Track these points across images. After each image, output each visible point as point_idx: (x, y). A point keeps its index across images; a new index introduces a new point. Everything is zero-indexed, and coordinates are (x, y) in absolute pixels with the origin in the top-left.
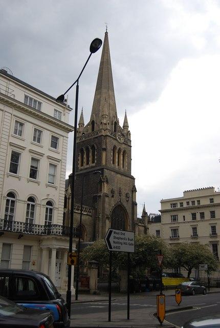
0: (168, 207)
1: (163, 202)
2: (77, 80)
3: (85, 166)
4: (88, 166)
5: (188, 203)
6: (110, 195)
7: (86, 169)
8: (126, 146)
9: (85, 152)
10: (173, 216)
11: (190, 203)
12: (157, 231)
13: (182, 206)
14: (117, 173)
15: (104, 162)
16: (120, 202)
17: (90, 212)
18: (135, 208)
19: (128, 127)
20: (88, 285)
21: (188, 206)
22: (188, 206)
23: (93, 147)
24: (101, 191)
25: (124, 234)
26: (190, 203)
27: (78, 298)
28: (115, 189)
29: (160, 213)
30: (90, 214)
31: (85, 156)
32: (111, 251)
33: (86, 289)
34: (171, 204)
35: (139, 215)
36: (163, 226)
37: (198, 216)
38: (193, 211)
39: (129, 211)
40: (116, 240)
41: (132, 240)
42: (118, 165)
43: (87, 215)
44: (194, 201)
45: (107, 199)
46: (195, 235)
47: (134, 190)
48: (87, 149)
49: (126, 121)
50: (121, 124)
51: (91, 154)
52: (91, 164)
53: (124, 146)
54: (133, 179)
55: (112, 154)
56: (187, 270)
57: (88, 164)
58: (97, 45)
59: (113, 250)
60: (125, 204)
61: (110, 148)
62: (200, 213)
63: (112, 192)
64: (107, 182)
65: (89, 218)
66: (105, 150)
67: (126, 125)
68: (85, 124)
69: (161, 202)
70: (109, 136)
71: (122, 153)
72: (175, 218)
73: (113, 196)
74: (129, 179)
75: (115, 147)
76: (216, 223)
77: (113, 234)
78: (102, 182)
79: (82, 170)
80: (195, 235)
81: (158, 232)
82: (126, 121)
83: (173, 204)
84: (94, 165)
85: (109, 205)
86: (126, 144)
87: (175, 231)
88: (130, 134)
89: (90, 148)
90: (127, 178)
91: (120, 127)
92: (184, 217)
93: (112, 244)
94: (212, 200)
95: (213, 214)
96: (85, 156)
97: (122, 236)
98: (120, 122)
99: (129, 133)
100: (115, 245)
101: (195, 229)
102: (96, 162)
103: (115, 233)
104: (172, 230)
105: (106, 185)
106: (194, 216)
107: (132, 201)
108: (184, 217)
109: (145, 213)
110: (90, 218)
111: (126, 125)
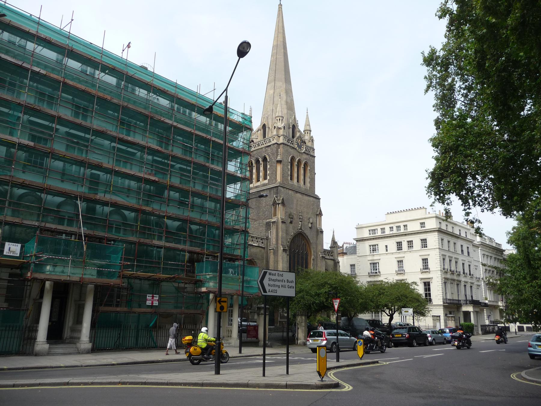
0: (366, 234)
2: (226, 90)
4: (259, 184)
5: (391, 228)
7: (257, 187)
8: (307, 157)
10: (373, 246)
11: (395, 228)
12: (351, 265)
13: (384, 232)
16: (301, 229)
20: (256, 336)
21: (391, 232)
22: (391, 232)
23: (265, 159)
25: (282, 275)
26: (395, 228)
27: (242, 352)
28: (294, 212)
29: (355, 242)
30: (262, 245)
32: (266, 296)
33: (254, 339)
34: (370, 230)
35: (327, 245)
36: (360, 259)
37: (405, 245)
38: (398, 239)
40: (272, 283)
41: (292, 282)
42: (298, 181)
44: (392, 227)
46: (401, 270)
49: (308, 124)
50: (301, 127)
53: (305, 156)
54: (318, 199)
55: (289, 167)
56: (388, 315)
57: (258, 180)
58: (246, 48)
59: (268, 294)
60: (308, 232)
62: (408, 242)
63: (291, 216)
65: (260, 251)
71: (296, 163)
72: (374, 249)
74: (312, 199)
75: (293, 159)
77: (267, 276)
78: (276, 204)
80: (401, 270)
81: (353, 266)
82: (308, 124)
83: (372, 230)
86: (308, 154)
87: (374, 265)
89: (260, 160)
91: (299, 131)
92: (386, 246)
93: (267, 288)
94: (422, 224)
95: (424, 242)
97: (280, 278)
98: (299, 124)
100: (271, 288)
101: (400, 262)
102: (268, 177)
103: (270, 274)
104: (371, 264)
106: (399, 245)
108: (386, 246)
109: (334, 243)
111: (308, 128)
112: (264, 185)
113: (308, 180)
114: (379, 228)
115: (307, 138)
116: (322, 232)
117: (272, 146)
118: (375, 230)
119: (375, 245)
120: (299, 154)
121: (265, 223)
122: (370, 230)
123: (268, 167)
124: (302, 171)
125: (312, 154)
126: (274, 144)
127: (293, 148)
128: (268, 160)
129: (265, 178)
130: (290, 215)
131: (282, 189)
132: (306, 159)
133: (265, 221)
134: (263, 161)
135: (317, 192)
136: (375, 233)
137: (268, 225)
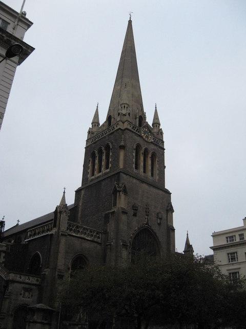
0: (223, 242)
1: (215, 236)
3: (97, 174)
6: (132, 212)
7: (98, 177)
9: (97, 155)
10: (231, 254)
14: (143, 181)
15: (121, 166)
16: (147, 224)
17: (99, 237)
18: (172, 234)
19: (160, 124)
23: (108, 148)
24: (115, 204)
29: (211, 252)
30: (99, 240)
31: (97, 161)
34: (227, 238)
35: (180, 248)
39: (162, 238)
43: (93, 241)
45: (124, 217)
47: (170, 210)
48: (100, 152)
49: (156, 117)
50: (150, 120)
51: (104, 157)
52: (104, 171)
53: (152, 147)
54: (168, 193)
55: (134, 154)
57: (100, 171)
60: (155, 228)
61: (131, 146)
63: (135, 208)
64: (125, 191)
66: (123, 147)
67: (156, 123)
68: (101, 125)
69: (213, 236)
70: (130, 130)
71: (150, 156)
73: (135, 215)
74: (161, 192)
75: (138, 147)
76: (240, 268)
79: (92, 180)
82: (156, 117)
83: (230, 237)
84: (108, 170)
85: (128, 228)
88: (162, 133)
89: (103, 148)
90: (157, 191)
91: (147, 125)
96: (97, 161)
98: (147, 115)
99: (160, 133)
102: (110, 165)
105: (123, 196)
107: (167, 225)
110: (99, 247)
111: (156, 121)
112: (106, 174)
113: (156, 172)
114: (237, 235)
115: (155, 130)
116: (173, 230)
117: (115, 133)
118: (232, 237)
119: (234, 253)
120: (146, 143)
121: (104, 215)
122: (227, 238)
123: (111, 154)
124: (149, 162)
125: (161, 146)
126: (117, 130)
127: (140, 136)
128: (111, 147)
129: (107, 167)
130: (133, 206)
131: (124, 176)
132: (154, 149)
133: (103, 214)
134: (106, 149)
135: (167, 186)
136: (233, 240)
137: (107, 218)
